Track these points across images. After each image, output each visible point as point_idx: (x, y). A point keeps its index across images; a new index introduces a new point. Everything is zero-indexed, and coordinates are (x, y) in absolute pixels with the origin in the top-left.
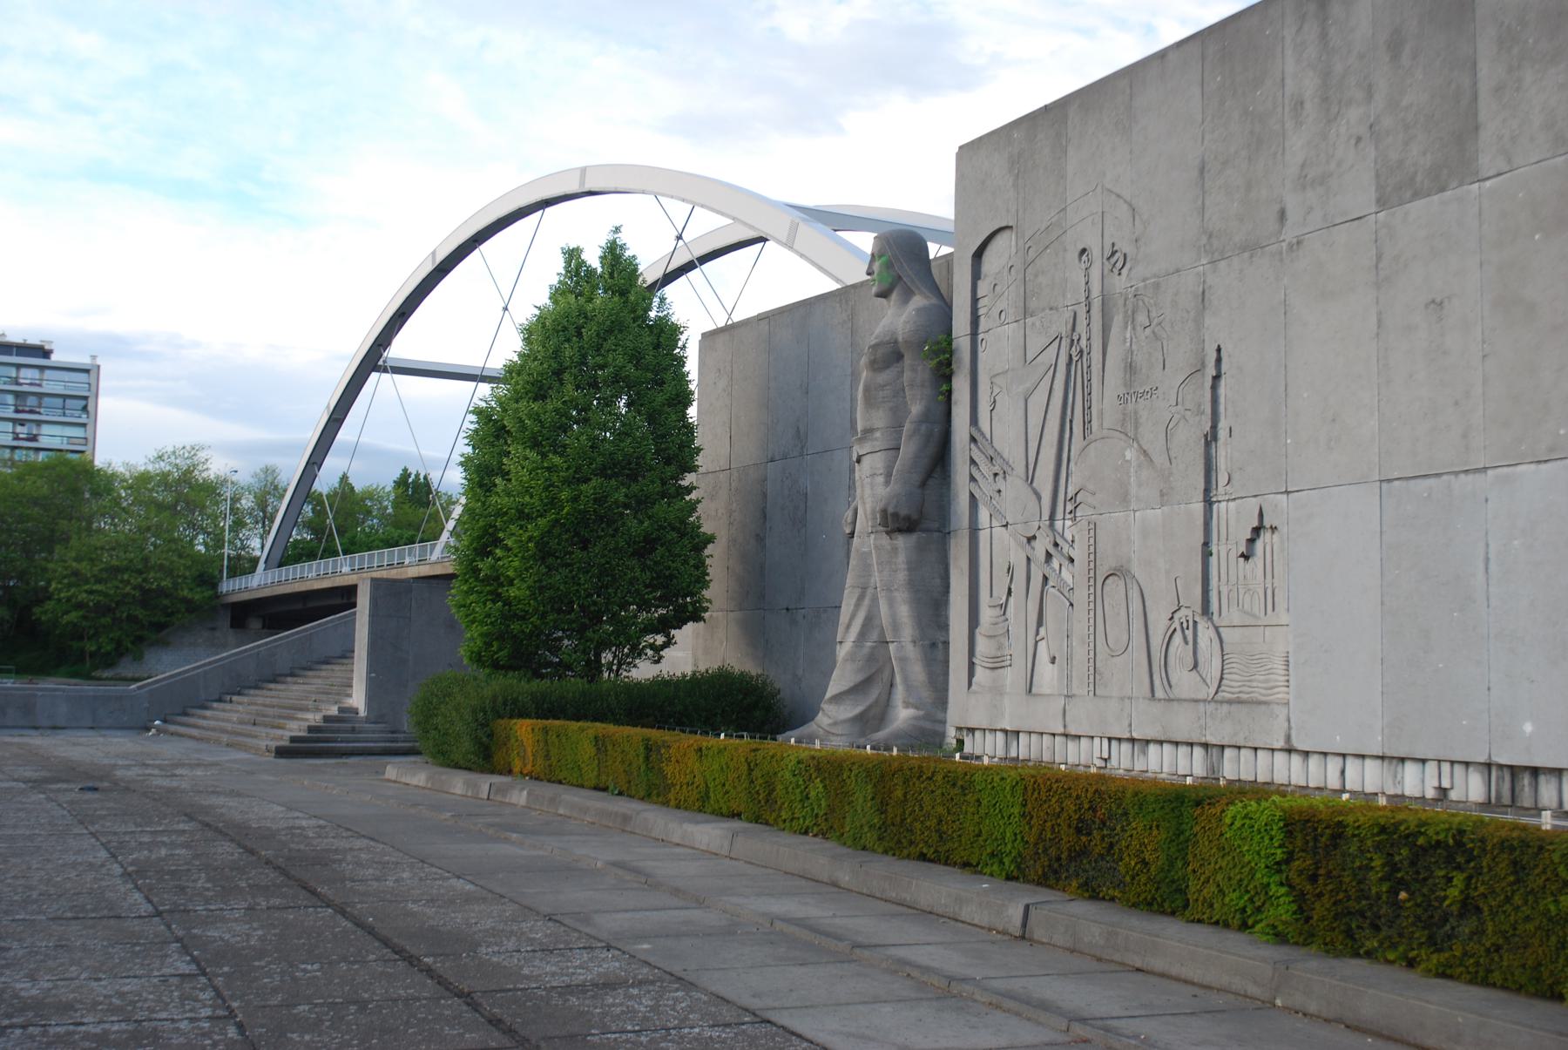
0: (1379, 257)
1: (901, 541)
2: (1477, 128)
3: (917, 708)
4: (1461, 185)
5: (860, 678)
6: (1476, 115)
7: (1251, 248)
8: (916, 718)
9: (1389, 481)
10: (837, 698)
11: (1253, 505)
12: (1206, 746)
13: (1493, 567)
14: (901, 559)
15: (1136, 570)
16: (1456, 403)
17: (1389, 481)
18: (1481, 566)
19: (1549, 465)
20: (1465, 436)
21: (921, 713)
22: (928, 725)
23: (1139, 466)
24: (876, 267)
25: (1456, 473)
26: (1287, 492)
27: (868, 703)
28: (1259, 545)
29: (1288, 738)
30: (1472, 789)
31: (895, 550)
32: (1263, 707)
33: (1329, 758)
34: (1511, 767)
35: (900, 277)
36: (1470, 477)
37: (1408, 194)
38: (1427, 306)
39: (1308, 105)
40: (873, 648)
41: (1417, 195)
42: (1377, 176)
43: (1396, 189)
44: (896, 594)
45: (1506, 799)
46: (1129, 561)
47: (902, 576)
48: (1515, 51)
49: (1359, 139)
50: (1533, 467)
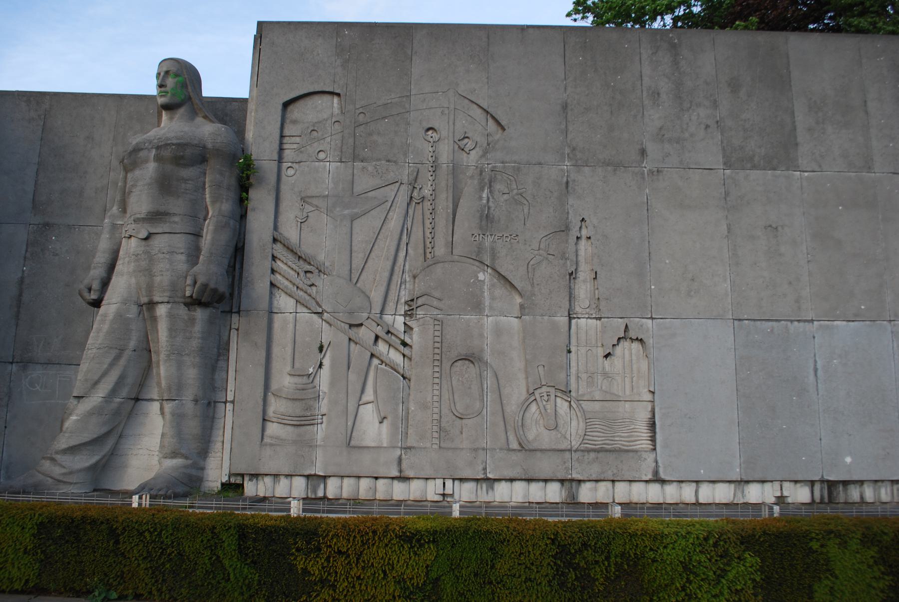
0: (727, 194)
1: (200, 314)
2: (797, 145)
3: (186, 458)
4: (788, 169)
5: (104, 430)
6: (796, 137)
7: (616, 165)
8: (186, 467)
9: (740, 320)
10: (72, 450)
11: (621, 323)
12: (562, 481)
13: (820, 373)
14: (198, 328)
15: (488, 357)
16: (790, 283)
17: (740, 320)
18: (812, 372)
19: (856, 323)
20: (797, 301)
21: (190, 462)
22: (194, 472)
23: (493, 285)
24: (170, 82)
25: (792, 321)
26: (652, 318)
27: (102, 453)
28: (619, 349)
29: (656, 472)
30: (801, 495)
31: (192, 321)
32: (631, 454)
33: (617, 484)
34: (828, 481)
35: (190, 98)
36: (802, 324)
37: (749, 165)
38: (765, 228)
39: (664, 96)
40: (122, 403)
41: (754, 167)
42: (724, 149)
43: (735, 159)
44: (186, 358)
45: (826, 500)
46: (482, 350)
47: (195, 343)
48: (820, 114)
49: (707, 127)
50: (844, 323)
